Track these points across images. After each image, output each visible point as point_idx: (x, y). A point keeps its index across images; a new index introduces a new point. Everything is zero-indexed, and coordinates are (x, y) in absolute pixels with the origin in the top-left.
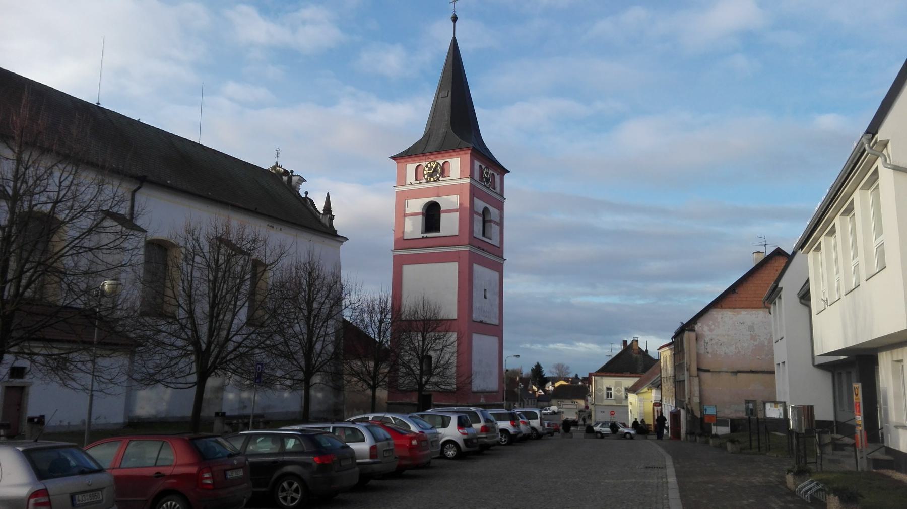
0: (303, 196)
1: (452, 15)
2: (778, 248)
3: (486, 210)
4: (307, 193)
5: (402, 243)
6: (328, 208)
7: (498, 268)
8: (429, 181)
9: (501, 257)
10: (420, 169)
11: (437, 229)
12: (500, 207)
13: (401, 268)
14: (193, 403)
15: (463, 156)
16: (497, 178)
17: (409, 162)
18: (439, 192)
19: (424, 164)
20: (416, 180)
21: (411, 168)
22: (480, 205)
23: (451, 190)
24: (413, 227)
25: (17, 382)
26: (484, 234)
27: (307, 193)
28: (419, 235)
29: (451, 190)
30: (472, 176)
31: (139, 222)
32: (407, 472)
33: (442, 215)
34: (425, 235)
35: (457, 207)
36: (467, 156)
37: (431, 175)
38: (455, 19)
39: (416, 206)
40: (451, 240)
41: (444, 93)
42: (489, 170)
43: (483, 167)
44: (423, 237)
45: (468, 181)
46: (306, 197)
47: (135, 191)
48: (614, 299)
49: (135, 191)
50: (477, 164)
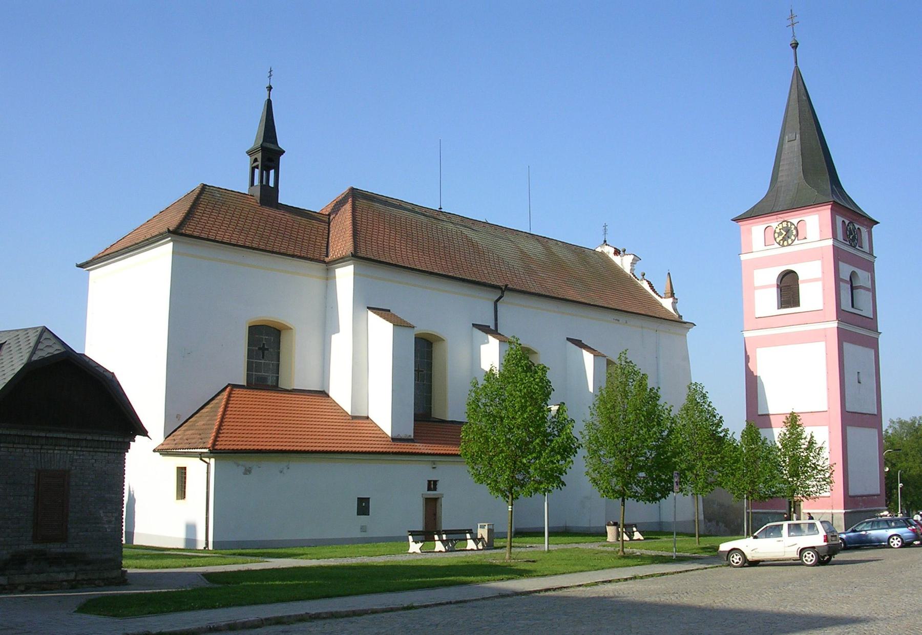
2: (358, 514)
3: (853, 275)
7: (873, 344)
8: (783, 246)
9: (875, 329)
11: (797, 304)
12: (869, 267)
16: (864, 231)
22: (846, 270)
25: (432, 494)
26: (853, 306)
30: (835, 237)
31: (684, 319)
32: (838, 557)
36: (826, 212)
38: (795, 46)
42: (853, 226)
43: (847, 222)
45: (830, 242)
47: (497, 301)
48: (581, 546)
49: (497, 301)
50: (839, 220)
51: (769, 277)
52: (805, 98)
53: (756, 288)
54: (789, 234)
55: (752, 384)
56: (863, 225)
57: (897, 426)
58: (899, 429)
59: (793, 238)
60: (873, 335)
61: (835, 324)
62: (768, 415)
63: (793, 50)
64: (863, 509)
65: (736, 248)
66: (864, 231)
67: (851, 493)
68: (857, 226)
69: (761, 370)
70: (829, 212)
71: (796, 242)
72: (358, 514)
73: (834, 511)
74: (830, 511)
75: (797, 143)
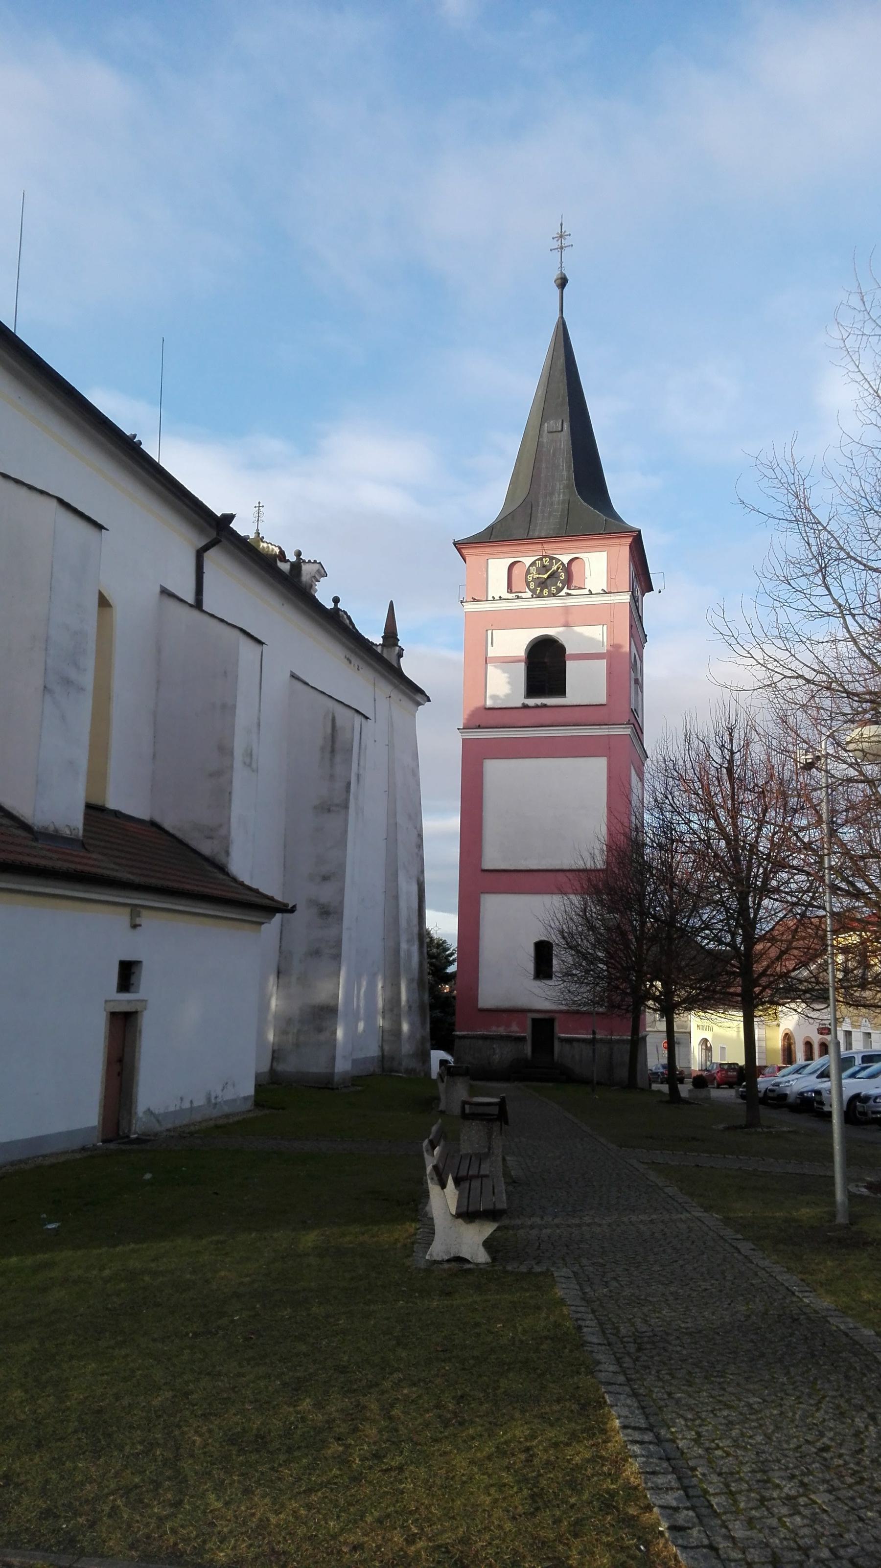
0: (330, 605)
1: (556, 274)
4: (336, 600)
5: (484, 718)
6: (391, 636)
8: (540, 596)
10: (516, 570)
13: (482, 765)
14: (648, 1056)
15: (615, 549)
17: (496, 556)
18: (567, 618)
19: (528, 561)
20: (510, 589)
21: (497, 567)
23: (591, 616)
24: (504, 686)
27: (336, 600)
28: (519, 699)
29: (591, 616)
33: (570, 665)
34: (532, 702)
35: (604, 650)
37: (543, 584)
38: (563, 282)
39: (514, 643)
40: (587, 714)
41: (553, 424)
44: (525, 706)
46: (336, 610)
47: (206, 548)
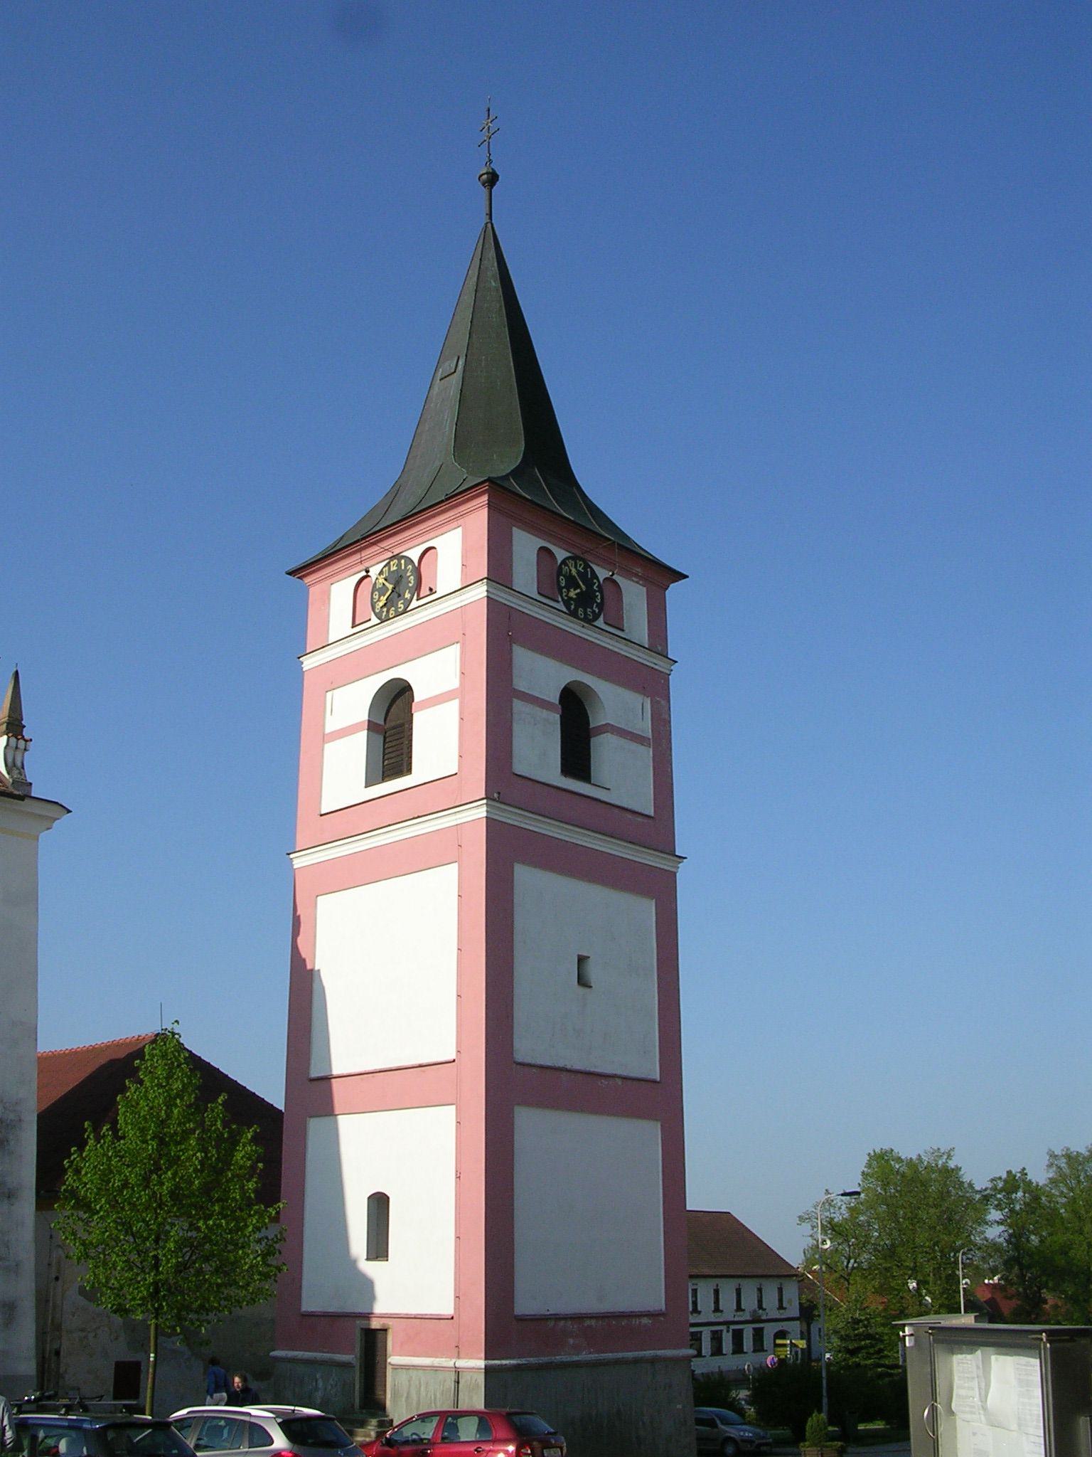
2: (118, 1365)
7: (661, 890)
9: (667, 847)
16: (634, 595)
38: (492, 179)
43: (561, 554)
50: (526, 545)
51: (351, 705)
52: (495, 284)
53: (326, 738)
54: (400, 589)
55: (303, 988)
56: (628, 574)
57: (1063, 1163)
58: (1067, 1171)
59: (407, 596)
60: (512, 817)
61: (481, 812)
62: (327, 1079)
63: (485, 191)
64: (584, 1356)
65: (294, 635)
66: (634, 595)
67: (525, 1304)
68: (602, 573)
69: (326, 959)
70: (483, 514)
71: (414, 603)
72: (118, 1365)
73: (461, 1363)
74: (451, 1364)
75: (456, 380)
